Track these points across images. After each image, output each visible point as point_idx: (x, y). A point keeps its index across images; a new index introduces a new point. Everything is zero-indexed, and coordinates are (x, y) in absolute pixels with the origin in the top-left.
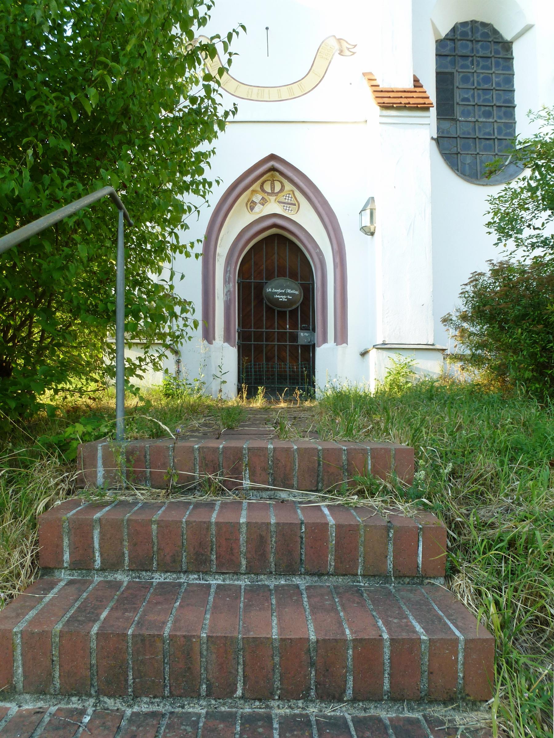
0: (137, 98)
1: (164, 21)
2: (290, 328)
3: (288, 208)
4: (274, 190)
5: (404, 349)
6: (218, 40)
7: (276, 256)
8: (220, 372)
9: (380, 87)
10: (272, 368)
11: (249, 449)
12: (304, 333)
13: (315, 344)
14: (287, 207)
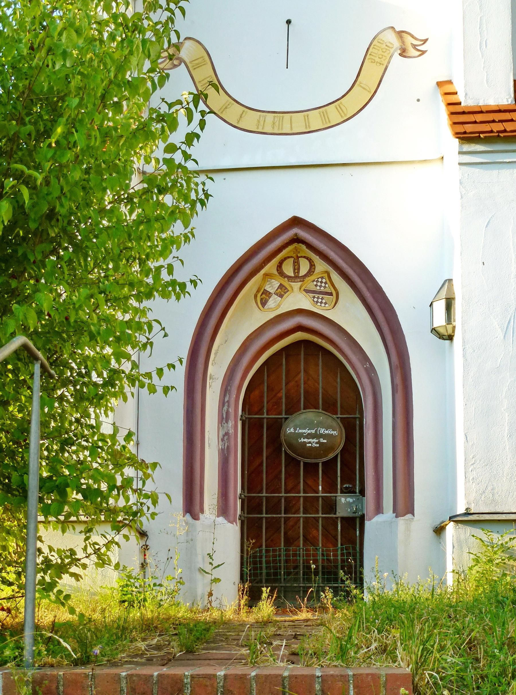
0: (66, 197)
1: (104, 92)
2: (324, 491)
3: (320, 300)
4: (298, 272)
5: (499, 520)
6: (178, 107)
7: (302, 374)
8: (211, 563)
9: (462, 104)
10: (295, 555)
11: (192, 677)
12: (346, 497)
13: (364, 515)
14: (318, 298)
